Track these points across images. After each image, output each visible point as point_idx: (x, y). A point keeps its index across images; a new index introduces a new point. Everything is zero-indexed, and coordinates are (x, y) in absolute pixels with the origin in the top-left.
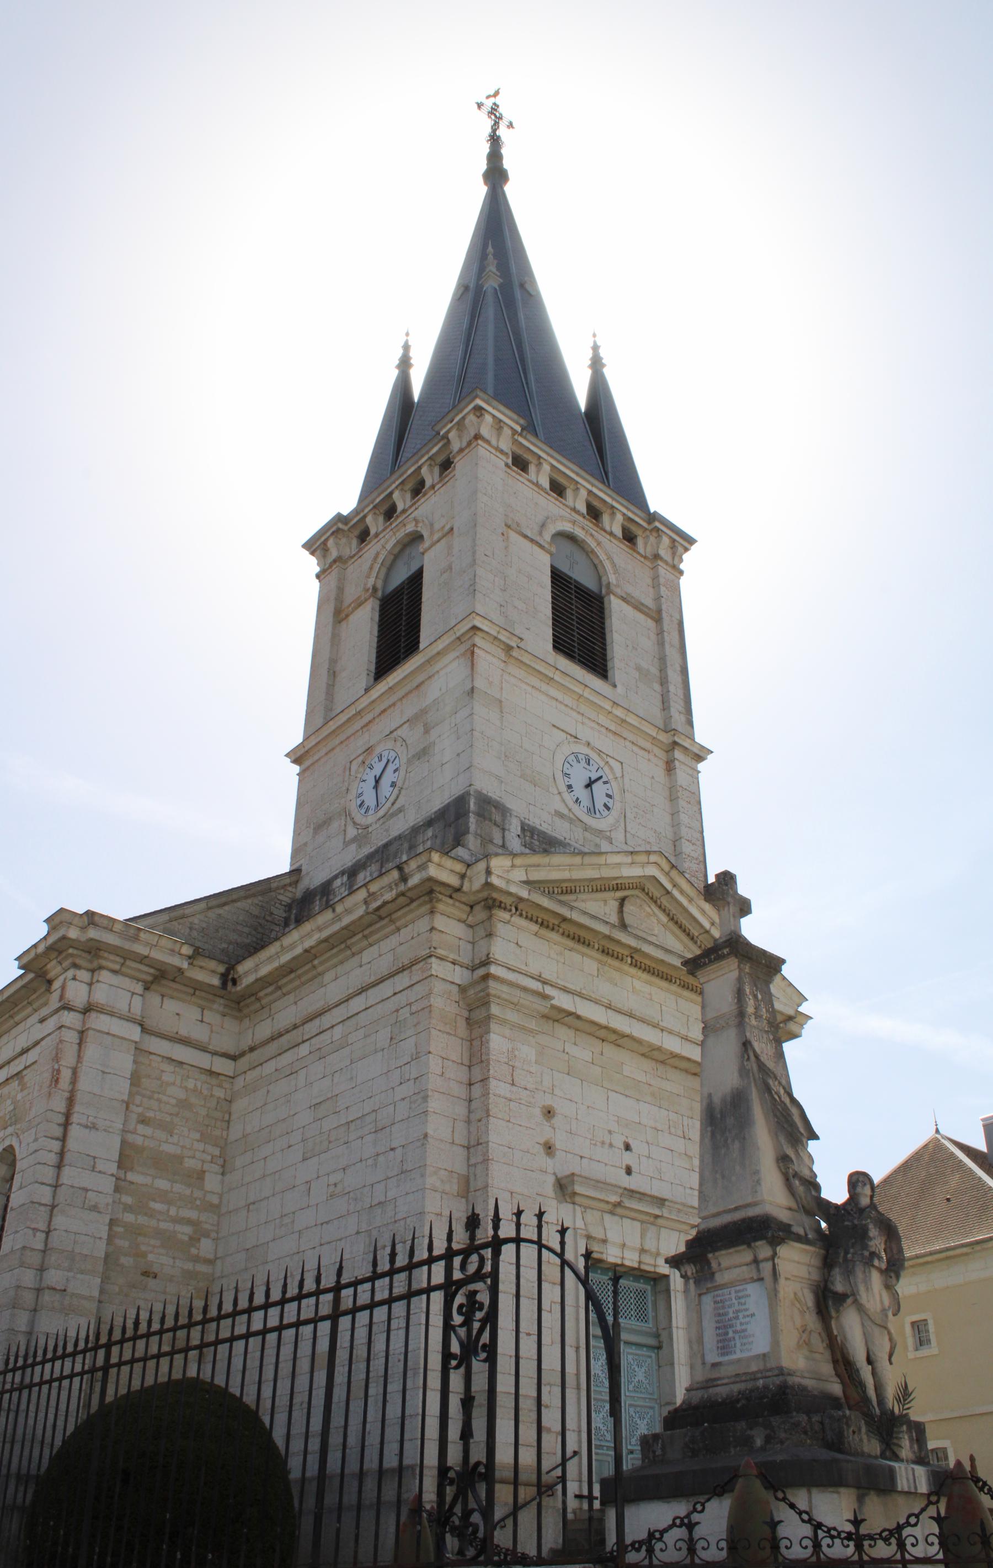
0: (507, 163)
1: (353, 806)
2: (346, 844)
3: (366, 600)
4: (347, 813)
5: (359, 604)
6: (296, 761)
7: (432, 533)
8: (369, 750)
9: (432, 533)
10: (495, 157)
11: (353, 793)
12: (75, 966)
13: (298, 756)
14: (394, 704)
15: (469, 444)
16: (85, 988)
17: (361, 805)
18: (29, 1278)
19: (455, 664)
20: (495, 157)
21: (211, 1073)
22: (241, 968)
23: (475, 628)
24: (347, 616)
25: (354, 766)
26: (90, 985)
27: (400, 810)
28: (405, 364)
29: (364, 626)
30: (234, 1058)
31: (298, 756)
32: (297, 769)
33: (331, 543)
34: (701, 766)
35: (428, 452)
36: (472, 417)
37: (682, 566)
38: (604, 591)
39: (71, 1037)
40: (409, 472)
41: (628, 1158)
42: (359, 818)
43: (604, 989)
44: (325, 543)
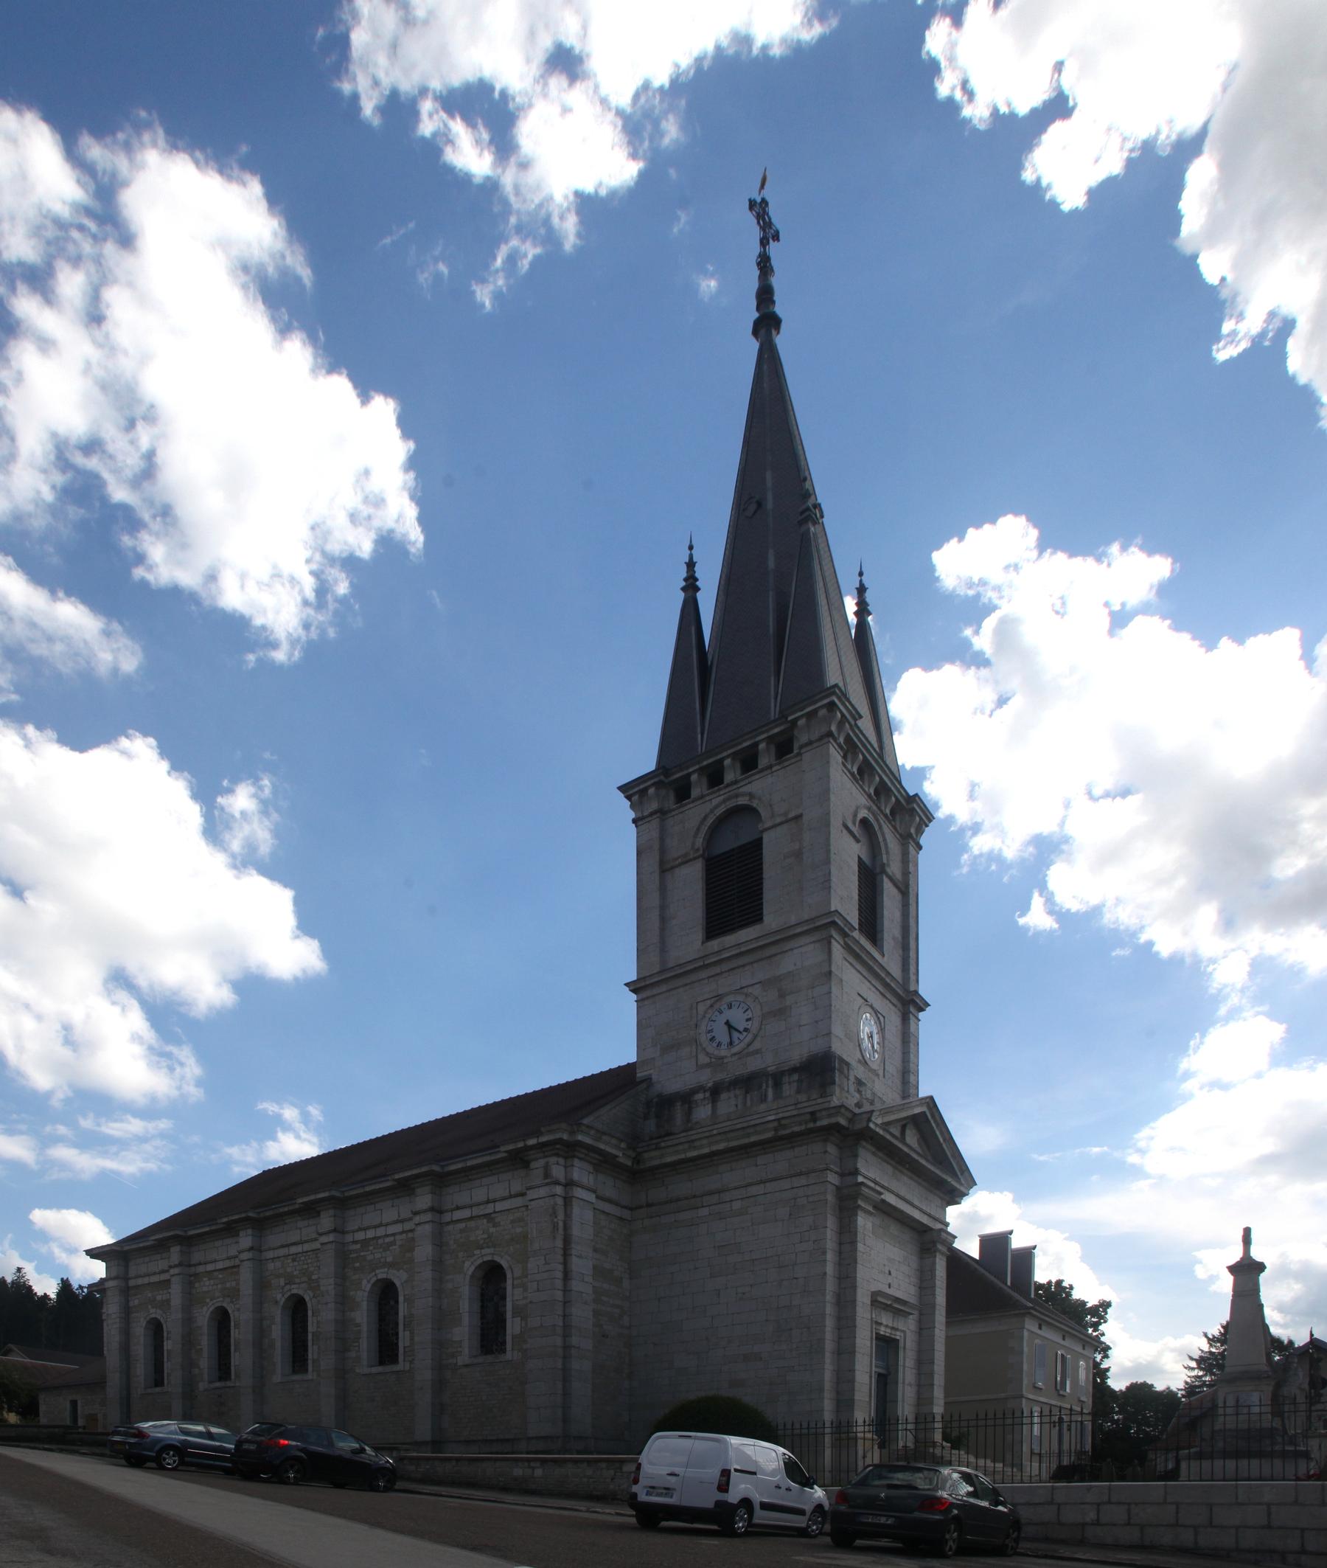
0: (781, 308)
1: (704, 1039)
2: (700, 1067)
3: (695, 859)
4: (695, 1041)
5: (686, 861)
6: (634, 991)
7: (773, 816)
8: (719, 997)
9: (773, 816)
10: (765, 295)
11: (703, 1028)
12: (557, 1155)
13: (635, 987)
14: (744, 966)
15: (821, 738)
16: (562, 1169)
17: (713, 1039)
18: (559, 1341)
19: (812, 946)
20: (765, 295)
21: (621, 1219)
22: (646, 1155)
23: (834, 923)
24: (672, 868)
25: (702, 1008)
26: (566, 1167)
27: (757, 1052)
28: (691, 586)
29: (690, 884)
30: (631, 1209)
31: (635, 987)
32: (634, 997)
33: (651, 791)
34: (921, 1015)
35: (767, 731)
36: (823, 712)
37: (922, 842)
38: (878, 870)
39: (560, 1201)
40: (745, 744)
41: (890, 1280)
42: (711, 1048)
43: (894, 1185)
44: (646, 789)
